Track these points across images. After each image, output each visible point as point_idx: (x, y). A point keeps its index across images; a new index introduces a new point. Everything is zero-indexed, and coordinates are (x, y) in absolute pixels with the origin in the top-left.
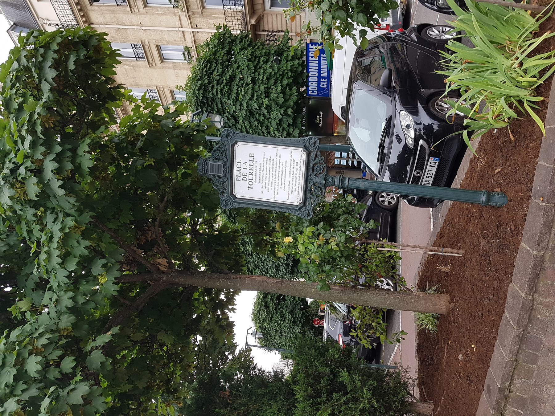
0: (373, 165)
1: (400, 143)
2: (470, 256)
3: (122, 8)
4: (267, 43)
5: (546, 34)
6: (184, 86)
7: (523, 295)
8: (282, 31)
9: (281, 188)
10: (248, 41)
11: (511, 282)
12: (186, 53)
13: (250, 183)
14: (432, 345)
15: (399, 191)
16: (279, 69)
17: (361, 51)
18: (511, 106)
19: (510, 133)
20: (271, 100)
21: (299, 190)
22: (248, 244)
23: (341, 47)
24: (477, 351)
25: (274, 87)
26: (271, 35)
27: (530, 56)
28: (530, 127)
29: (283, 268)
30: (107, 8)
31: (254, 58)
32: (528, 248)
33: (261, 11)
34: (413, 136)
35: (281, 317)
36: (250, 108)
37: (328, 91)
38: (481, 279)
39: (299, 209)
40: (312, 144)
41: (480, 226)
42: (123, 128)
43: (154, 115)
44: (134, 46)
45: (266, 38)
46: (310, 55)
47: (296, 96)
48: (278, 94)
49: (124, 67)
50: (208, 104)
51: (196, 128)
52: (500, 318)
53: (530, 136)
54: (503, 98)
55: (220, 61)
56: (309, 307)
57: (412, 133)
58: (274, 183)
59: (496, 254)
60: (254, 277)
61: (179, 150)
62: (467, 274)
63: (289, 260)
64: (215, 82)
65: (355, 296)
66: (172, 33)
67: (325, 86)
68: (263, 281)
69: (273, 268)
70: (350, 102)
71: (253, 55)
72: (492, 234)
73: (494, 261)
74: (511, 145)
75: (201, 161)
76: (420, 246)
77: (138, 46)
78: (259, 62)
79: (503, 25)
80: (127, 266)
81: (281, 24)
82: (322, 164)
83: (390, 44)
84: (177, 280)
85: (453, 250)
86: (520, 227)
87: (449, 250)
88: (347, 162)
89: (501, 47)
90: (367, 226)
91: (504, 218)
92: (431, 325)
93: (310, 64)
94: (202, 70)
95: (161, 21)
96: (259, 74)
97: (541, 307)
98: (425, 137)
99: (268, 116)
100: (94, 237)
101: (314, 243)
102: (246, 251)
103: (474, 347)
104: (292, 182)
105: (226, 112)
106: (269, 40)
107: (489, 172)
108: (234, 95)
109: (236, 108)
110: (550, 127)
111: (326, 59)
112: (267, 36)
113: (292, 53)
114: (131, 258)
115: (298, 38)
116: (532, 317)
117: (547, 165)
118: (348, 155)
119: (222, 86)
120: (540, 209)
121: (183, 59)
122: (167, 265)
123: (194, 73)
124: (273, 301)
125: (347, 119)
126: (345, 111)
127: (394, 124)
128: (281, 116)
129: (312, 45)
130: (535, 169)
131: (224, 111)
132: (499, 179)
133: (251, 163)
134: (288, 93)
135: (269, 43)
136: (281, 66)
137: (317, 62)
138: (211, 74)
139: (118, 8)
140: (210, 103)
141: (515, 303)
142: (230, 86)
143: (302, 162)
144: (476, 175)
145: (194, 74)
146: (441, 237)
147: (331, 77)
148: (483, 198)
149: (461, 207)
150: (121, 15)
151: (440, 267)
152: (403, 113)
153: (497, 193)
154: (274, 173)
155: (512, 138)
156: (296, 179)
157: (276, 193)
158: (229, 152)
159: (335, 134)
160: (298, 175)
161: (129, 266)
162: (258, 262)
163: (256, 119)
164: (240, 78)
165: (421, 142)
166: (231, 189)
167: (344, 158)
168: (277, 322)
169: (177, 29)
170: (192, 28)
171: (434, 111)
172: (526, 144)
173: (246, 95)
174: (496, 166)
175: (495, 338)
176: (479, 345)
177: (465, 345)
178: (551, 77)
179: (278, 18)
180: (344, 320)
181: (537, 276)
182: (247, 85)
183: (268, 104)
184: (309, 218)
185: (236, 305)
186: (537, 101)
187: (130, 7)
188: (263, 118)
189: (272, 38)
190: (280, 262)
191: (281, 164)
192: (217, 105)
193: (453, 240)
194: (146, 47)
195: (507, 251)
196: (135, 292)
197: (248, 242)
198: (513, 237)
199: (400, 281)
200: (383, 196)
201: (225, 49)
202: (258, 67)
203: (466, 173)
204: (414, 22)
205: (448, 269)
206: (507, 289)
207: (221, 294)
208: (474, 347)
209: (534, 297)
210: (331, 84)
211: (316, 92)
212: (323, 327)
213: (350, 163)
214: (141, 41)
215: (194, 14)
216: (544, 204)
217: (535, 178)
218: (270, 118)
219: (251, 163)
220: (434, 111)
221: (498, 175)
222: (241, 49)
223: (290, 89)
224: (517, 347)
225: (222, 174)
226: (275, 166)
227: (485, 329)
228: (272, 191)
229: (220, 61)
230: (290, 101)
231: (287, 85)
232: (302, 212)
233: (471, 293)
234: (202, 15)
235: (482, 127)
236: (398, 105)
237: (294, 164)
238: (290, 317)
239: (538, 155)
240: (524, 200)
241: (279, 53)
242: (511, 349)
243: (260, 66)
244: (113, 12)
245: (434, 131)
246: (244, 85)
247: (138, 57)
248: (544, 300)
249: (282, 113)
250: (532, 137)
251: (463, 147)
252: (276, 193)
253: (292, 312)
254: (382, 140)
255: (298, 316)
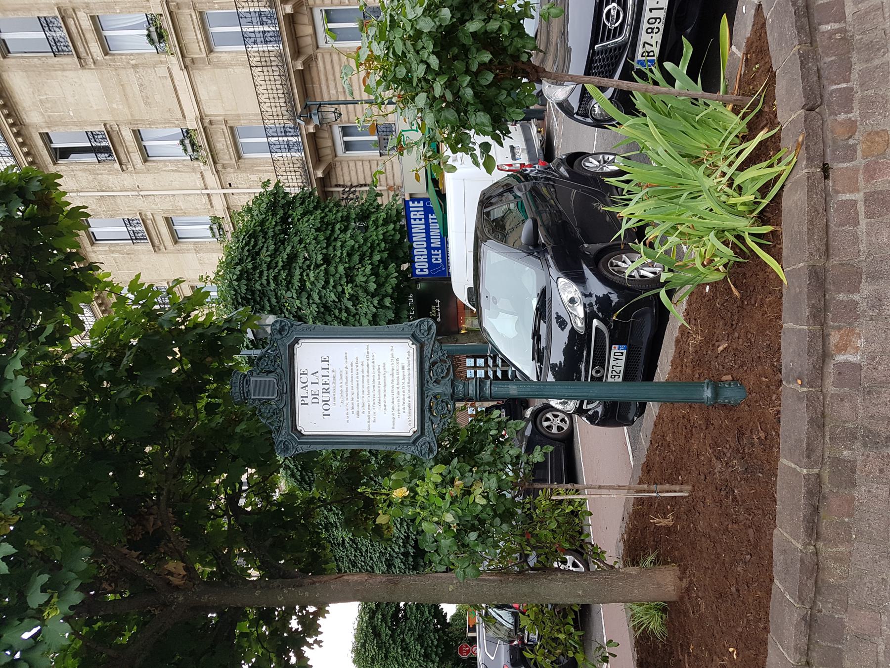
0: (529, 368)
1: (563, 329)
2: (701, 494)
3: (106, 166)
4: (343, 203)
5: (762, 133)
6: (212, 276)
7: (799, 546)
8: (365, 185)
9: (379, 409)
10: (313, 202)
11: (775, 526)
12: (215, 227)
13: (326, 407)
14: (663, 658)
15: (573, 394)
16: (366, 240)
17: (487, 199)
18: (726, 243)
19: (732, 286)
20: (356, 286)
21: (410, 409)
22: (336, 527)
23: (453, 169)
24: (740, 660)
25: (360, 266)
26: (349, 191)
27: (741, 168)
28: (761, 274)
29: (399, 561)
30: (82, 167)
31: (325, 226)
32: (793, 466)
33: (330, 157)
34: (582, 315)
35: (403, 649)
36: (324, 301)
37: (445, 267)
38: (727, 529)
39: (414, 442)
40: (425, 331)
41: (709, 441)
42: (97, 339)
43: (151, 310)
44: (129, 222)
45: (342, 196)
46: (412, 216)
47: (395, 277)
48: (368, 277)
49: (112, 255)
50: (255, 301)
51: (226, 326)
52: (769, 592)
53: (763, 287)
54: (712, 233)
55: (271, 234)
56: (449, 625)
57: (580, 311)
58: (366, 403)
59: (743, 482)
60: (345, 578)
61: (199, 368)
62: (702, 525)
63: (408, 545)
64: (265, 266)
65: (524, 588)
66: (191, 198)
67: (440, 261)
68: (361, 583)
69: (382, 562)
70: (479, 276)
71: (323, 221)
72: (730, 451)
73: (741, 495)
74: (736, 305)
75: (236, 379)
76: (619, 486)
77: (134, 222)
78: (333, 231)
79: (696, 128)
80: (110, 585)
81: (362, 175)
82: (445, 362)
83: (529, 184)
84: (205, 599)
85: (674, 487)
86: (774, 433)
87: (667, 486)
88: (486, 373)
89: (697, 161)
90: (531, 460)
91: (746, 421)
92: (655, 624)
93: (413, 231)
94: (243, 249)
95: (171, 181)
96: (335, 249)
97: (831, 564)
98: (600, 314)
99: (355, 311)
100: (40, 533)
101: (445, 494)
102: (333, 539)
103: (733, 652)
104: (398, 397)
105: (285, 310)
106: (347, 198)
107: (709, 352)
108: (297, 284)
109: (301, 303)
110: (791, 268)
111: (436, 221)
112: (343, 194)
113: (383, 215)
114: (117, 569)
115: (391, 193)
116: (820, 582)
117: (798, 327)
118: (486, 362)
119: (276, 270)
120: (799, 399)
121: (211, 235)
122: (185, 573)
123: (229, 254)
124: (386, 623)
125: (477, 305)
126: (474, 293)
127: (551, 299)
128: (374, 310)
129: (413, 203)
130: (780, 336)
131: (281, 309)
132: (727, 361)
133: (325, 372)
134: (383, 274)
135: (347, 203)
136: (368, 234)
137: (423, 227)
138: (258, 254)
139: (100, 165)
140: (258, 299)
141: (789, 561)
142: (289, 270)
143: (411, 362)
144: (690, 360)
145: (229, 256)
146: (649, 470)
147: (447, 248)
148: (708, 393)
149: (674, 415)
150: (105, 176)
151: (656, 520)
152: (563, 281)
153: (727, 383)
154: (366, 385)
155: (736, 293)
156: (404, 392)
157: (372, 419)
158: (285, 358)
159: (463, 332)
160: (406, 384)
161: (113, 584)
162: (355, 556)
163: (335, 316)
164: (306, 259)
165: (595, 322)
166: (292, 421)
167: (480, 367)
168: (396, 660)
169: (198, 192)
170: (223, 188)
171: (608, 275)
172: (758, 301)
173: (316, 282)
174: (717, 341)
175: (766, 629)
176: (741, 645)
177: (718, 650)
178: (779, 195)
179: (358, 167)
180: (511, 639)
181: (816, 510)
182: (317, 266)
183: (352, 292)
184: (431, 457)
185: (322, 633)
186: (765, 232)
187: (121, 164)
188: (346, 315)
189: (351, 196)
190: (393, 550)
191: (376, 368)
192: (269, 301)
193: (670, 471)
194: (149, 222)
195: (760, 475)
196: (128, 635)
197: (335, 522)
198: (765, 450)
199: (594, 553)
200: (548, 419)
201: (278, 216)
202: (333, 238)
203: (672, 362)
204: (561, 152)
205: (668, 521)
206: (771, 540)
207: (291, 619)
208: (733, 652)
209: (818, 547)
210: (448, 256)
211: (427, 270)
212: (476, 659)
213: (491, 374)
214: (140, 214)
215: (224, 166)
216: (805, 389)
217: (782, 350)
218: (357, 314)
219: (325, 372)
220: (608, 275)
221: (724, 355)
222: (304, 214)
223: (386, 268)
224: (805, 639)
225: (276, 395)
226: (365, 374)
227: (746, 616)
228: (364, 418)
229: (271, 234)
230: (387, 285)
231: (380, 261)
232: (419, 447)
233: (713, 557)
234: (239, 167)
235: (687, 282)
236: (554, 271)
237: (398, 366)
238: (418, 648)
239: (781, 315)
240: (772, 387)
241: (364, 216)
242: (797, 645)
243: (336, 236)
244: (92, 172)
245: (613, 304)
246: (312, 266)
247: (135, 238)
248: (834, 550)
249: (376, 305)
250: (766, 289)
251: (663, 315)
252: (372, 419)
253: (420, 639)
254: (535, 326)
255: (432, 643)
